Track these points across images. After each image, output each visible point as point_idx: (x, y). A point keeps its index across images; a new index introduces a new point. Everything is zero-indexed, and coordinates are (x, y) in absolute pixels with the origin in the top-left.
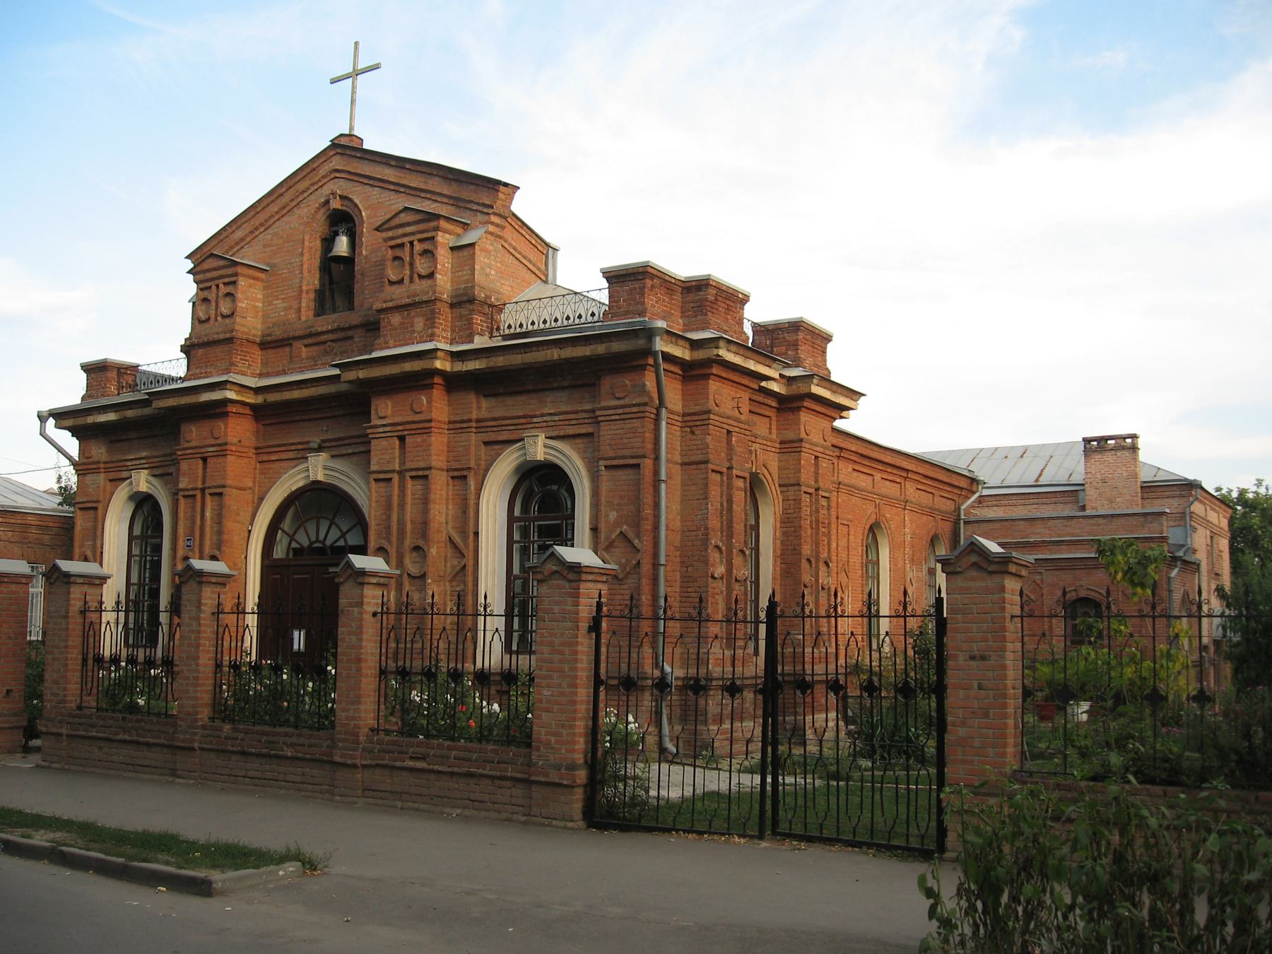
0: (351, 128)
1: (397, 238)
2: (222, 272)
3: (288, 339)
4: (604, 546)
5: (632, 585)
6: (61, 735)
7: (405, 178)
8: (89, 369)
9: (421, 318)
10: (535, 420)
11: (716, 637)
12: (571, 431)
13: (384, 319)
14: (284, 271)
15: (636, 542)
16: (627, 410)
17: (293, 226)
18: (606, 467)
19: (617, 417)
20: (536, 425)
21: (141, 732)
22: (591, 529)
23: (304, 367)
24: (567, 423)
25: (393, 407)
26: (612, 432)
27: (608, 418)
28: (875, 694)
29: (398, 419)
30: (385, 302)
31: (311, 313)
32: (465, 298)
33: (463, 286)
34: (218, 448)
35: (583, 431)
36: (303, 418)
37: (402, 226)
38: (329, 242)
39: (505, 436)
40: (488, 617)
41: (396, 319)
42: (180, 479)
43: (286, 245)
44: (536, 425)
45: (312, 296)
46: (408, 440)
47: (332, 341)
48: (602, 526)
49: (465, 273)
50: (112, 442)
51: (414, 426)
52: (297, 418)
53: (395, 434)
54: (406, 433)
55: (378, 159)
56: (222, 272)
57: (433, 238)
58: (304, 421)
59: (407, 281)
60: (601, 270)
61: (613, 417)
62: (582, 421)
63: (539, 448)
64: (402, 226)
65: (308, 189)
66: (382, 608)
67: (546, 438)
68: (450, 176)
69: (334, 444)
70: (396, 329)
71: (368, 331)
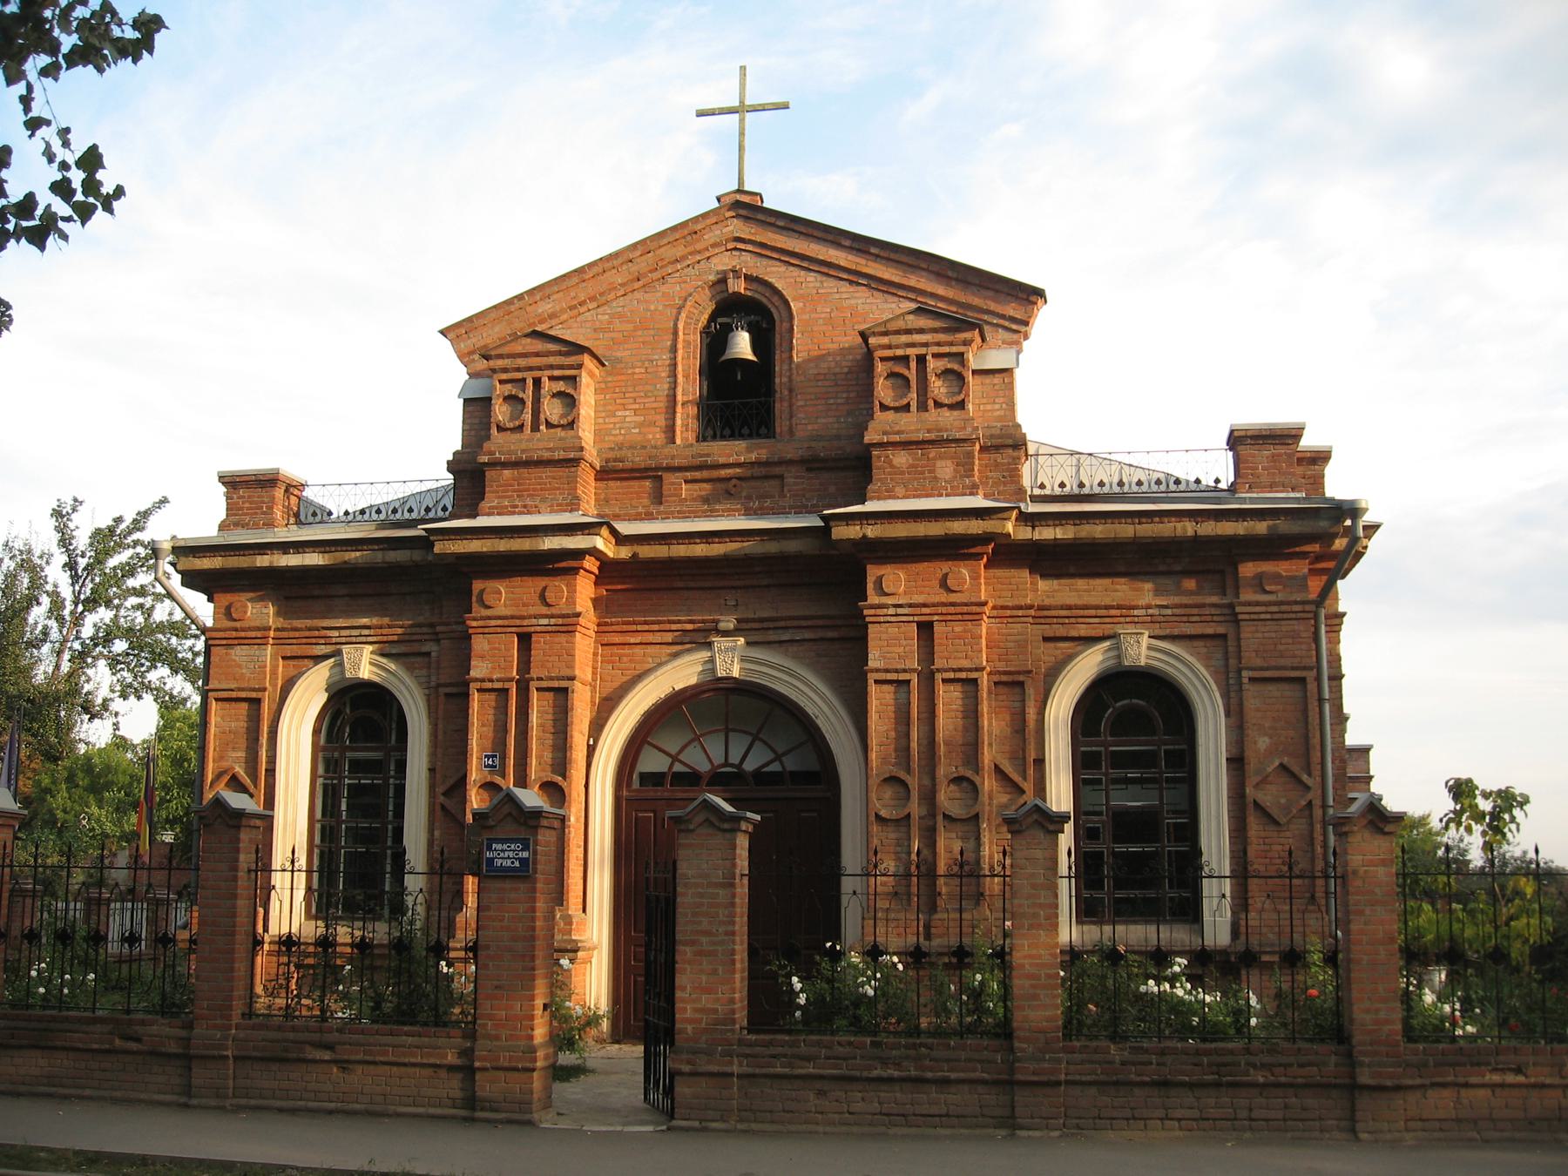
0: (741, 181)
1: (897, 347)
2: (552, 360)
3: (657, 469)
4: (1254, 783)
5: (1296, 832)
6: (732, 1075)
7: (866, 265)
8: (232, 482)
9: (949, 463)
10: (1136, 612)
11: (855, 893)
12: (1189, 629)
13: (879, 457)
14: (637, 370)
15: (1305, 777)
16: (1284, 608)
17: (652, 308)
18: (1250, 679)
19: (1268, 616)
20: (1136, 619)
21: (927, 1062)
22: (429, 769)
23: (689, 512)
24: (1185, 619)
25: (908, 581)
26: (1260, 635)
27: (1253, 616)
28: (293, 949)
29: (918, 599)
30: (885, 433)
31: (691, 437)
32: (1010, 442)
33: (999, 425)
34: (560, 621)
35: (1210, 631)
36: (692, 584)
37: (908, 332)
38: (716, 340)
39: (1083, 631)
40: (295, 873)
41: (901, 459)
42: (473, 663)
43: (640, 333)
44: (1136, 619)
45: (693, 410)
46: (937, 628)
47: (739, 479)
48: (1250, 755)
49: (997, 406)
50: (287, 598)
51: (952, 609)
52: (680, 584)
53: (513, 629)
54: (936, 618)
55: (816, 233)
56: (552, 360)
57: (962, 354)
58: (688, 589)
59: (528, 429)
60: (218, 473)
61: (1263, 616)
62: (1209, 618)
63: (365, 665)
64: (908, 332)
65: (684, 258)
66: (257, 865)
67: (1149, 637)
68: (950, 273)
69: (809, 623)
70: (903, 473)
71: (809, 470)
